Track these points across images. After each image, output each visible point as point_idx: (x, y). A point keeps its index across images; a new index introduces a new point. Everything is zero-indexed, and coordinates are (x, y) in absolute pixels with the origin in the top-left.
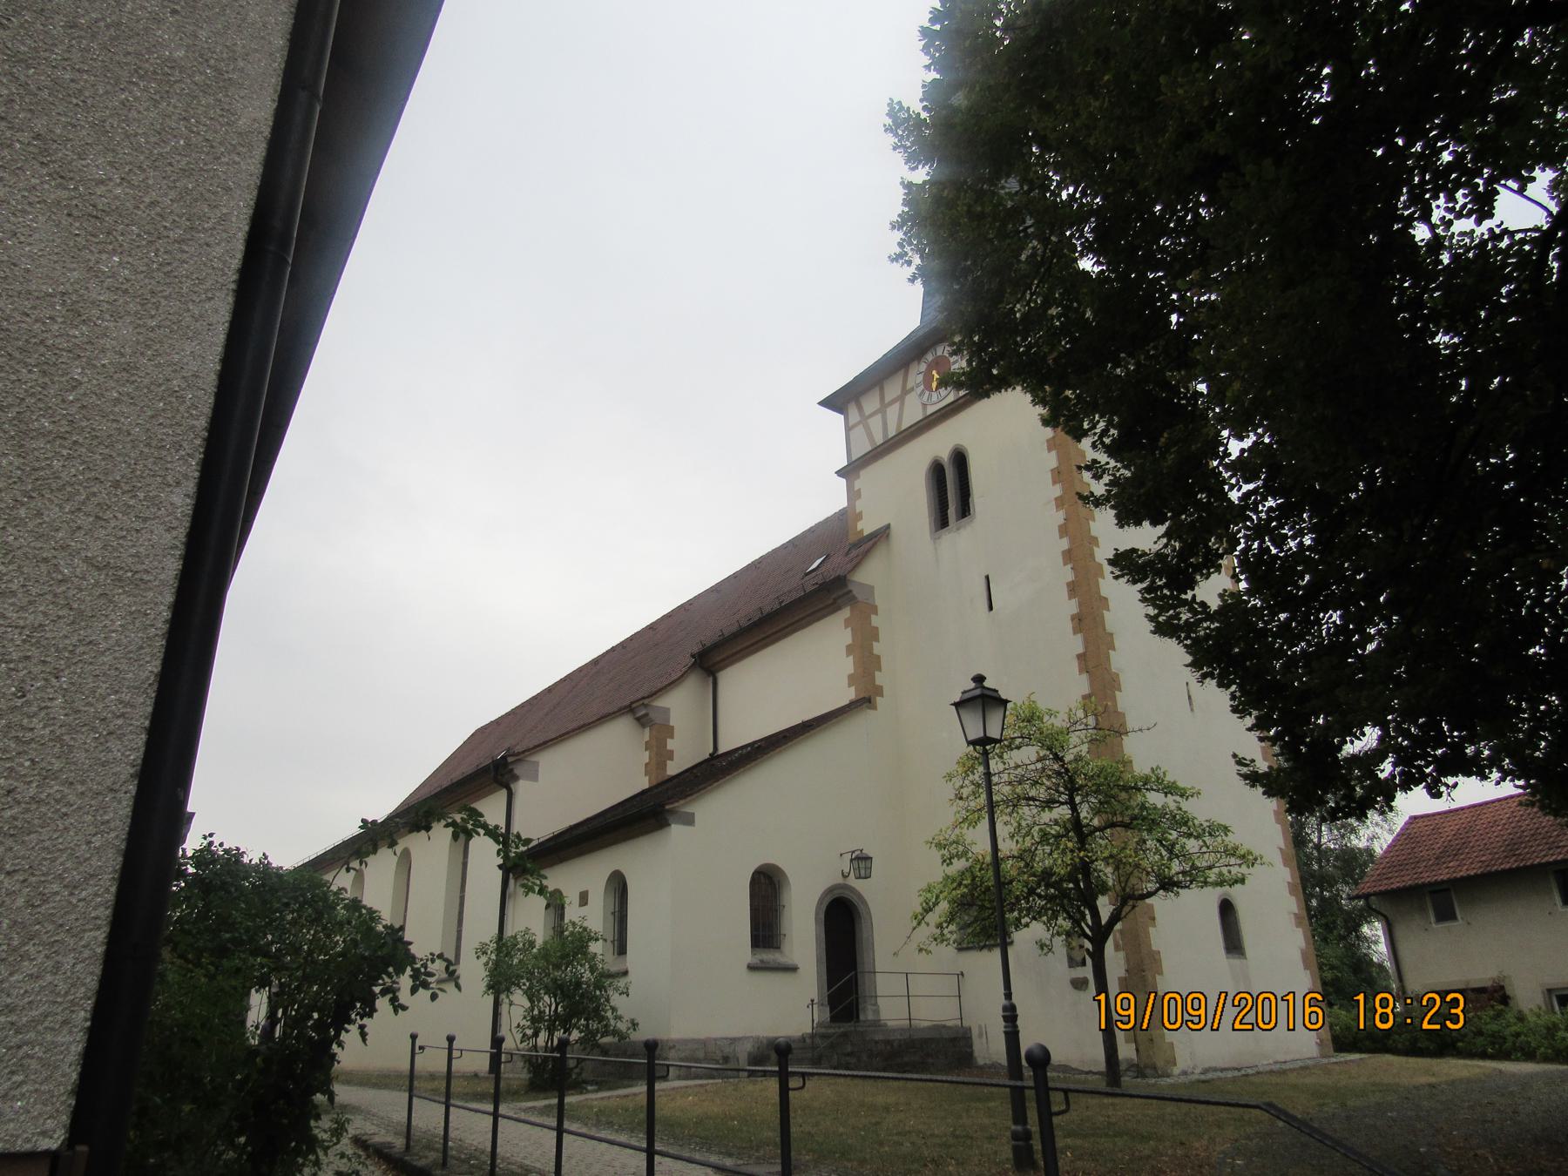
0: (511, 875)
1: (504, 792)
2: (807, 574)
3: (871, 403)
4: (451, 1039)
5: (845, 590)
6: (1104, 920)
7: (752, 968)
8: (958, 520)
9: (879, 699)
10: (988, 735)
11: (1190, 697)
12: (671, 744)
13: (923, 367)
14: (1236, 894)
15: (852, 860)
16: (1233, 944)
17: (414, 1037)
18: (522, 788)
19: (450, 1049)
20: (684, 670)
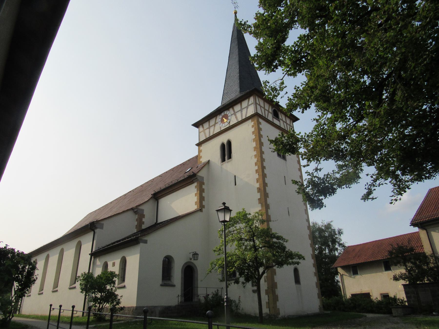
0: (93, 257)
1: (92, 233)
2: (186, 173)
3: (206, 125)
4: (73, 307)
5: (196, 178)
6: (261, 273)
7: (161, 285)
8: (228, 159)
9: (203, 209)
10: (225, 220)
11: (288, 212)
12: (144, 220)
13: (221, 117)
14: (299, 267)
15: (193, 255)
16: (297, 281)
17: (51, 305)
18: (97, 231)
19: (60, 309)
20: (149, 198)
